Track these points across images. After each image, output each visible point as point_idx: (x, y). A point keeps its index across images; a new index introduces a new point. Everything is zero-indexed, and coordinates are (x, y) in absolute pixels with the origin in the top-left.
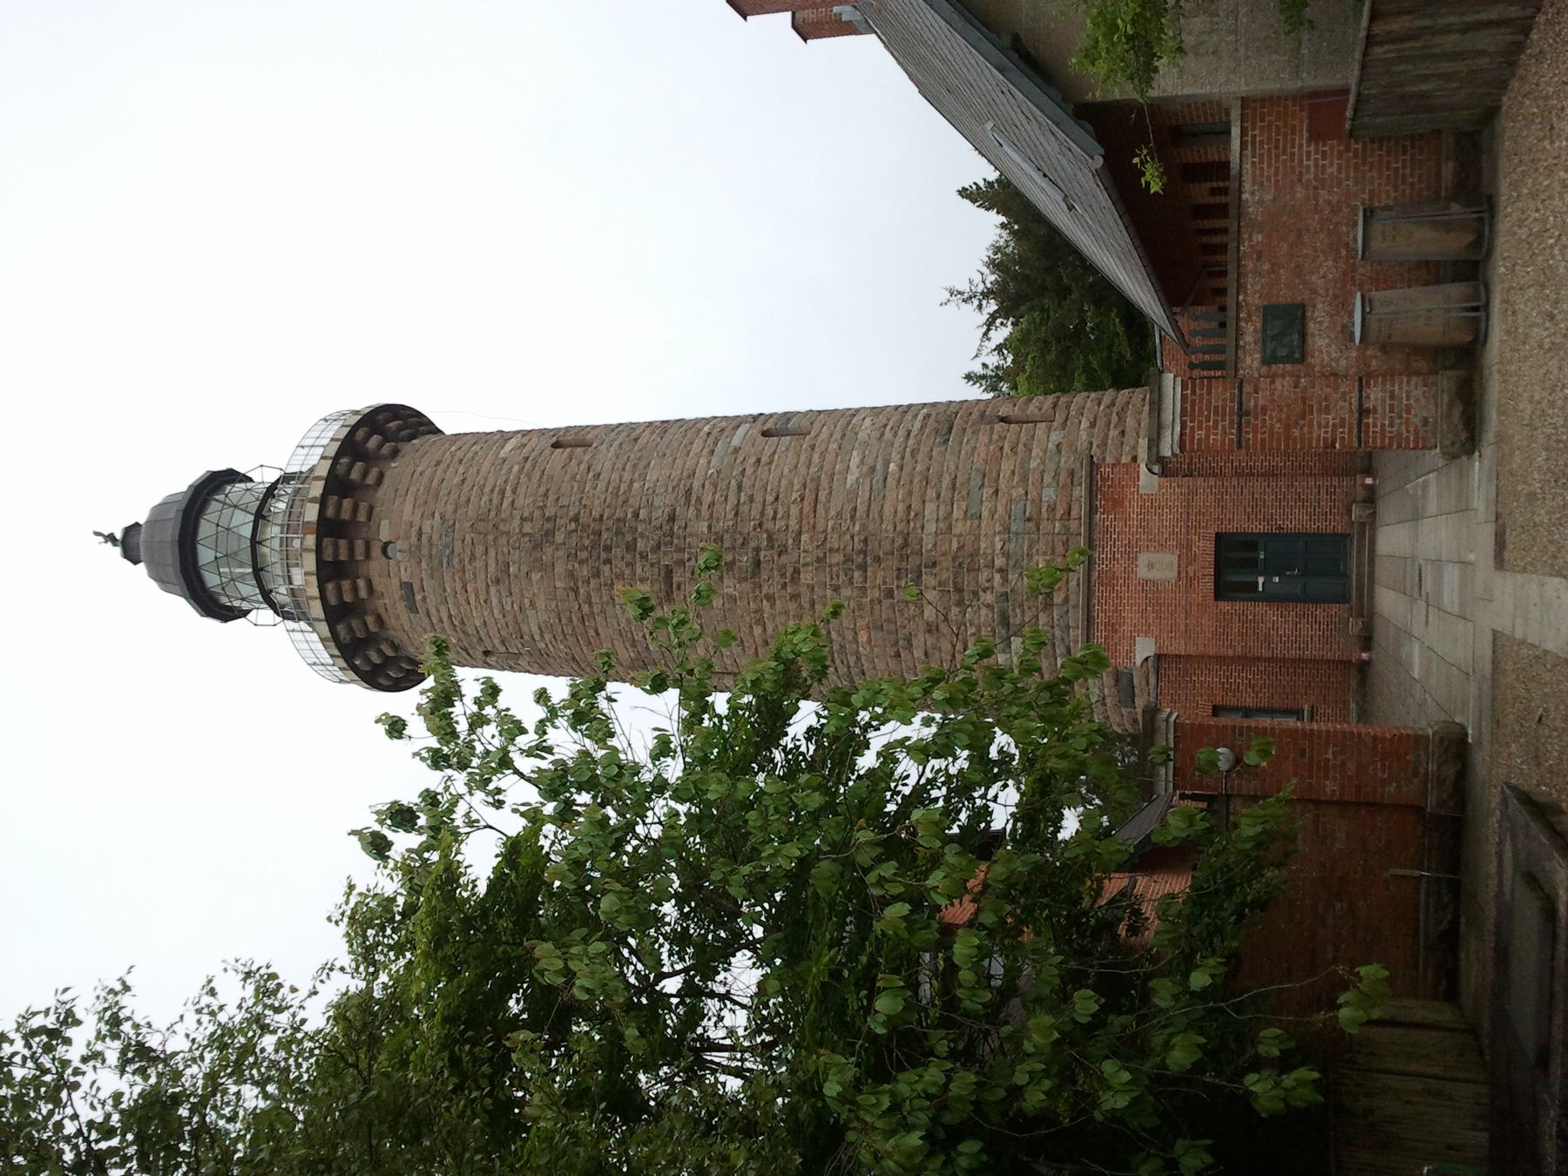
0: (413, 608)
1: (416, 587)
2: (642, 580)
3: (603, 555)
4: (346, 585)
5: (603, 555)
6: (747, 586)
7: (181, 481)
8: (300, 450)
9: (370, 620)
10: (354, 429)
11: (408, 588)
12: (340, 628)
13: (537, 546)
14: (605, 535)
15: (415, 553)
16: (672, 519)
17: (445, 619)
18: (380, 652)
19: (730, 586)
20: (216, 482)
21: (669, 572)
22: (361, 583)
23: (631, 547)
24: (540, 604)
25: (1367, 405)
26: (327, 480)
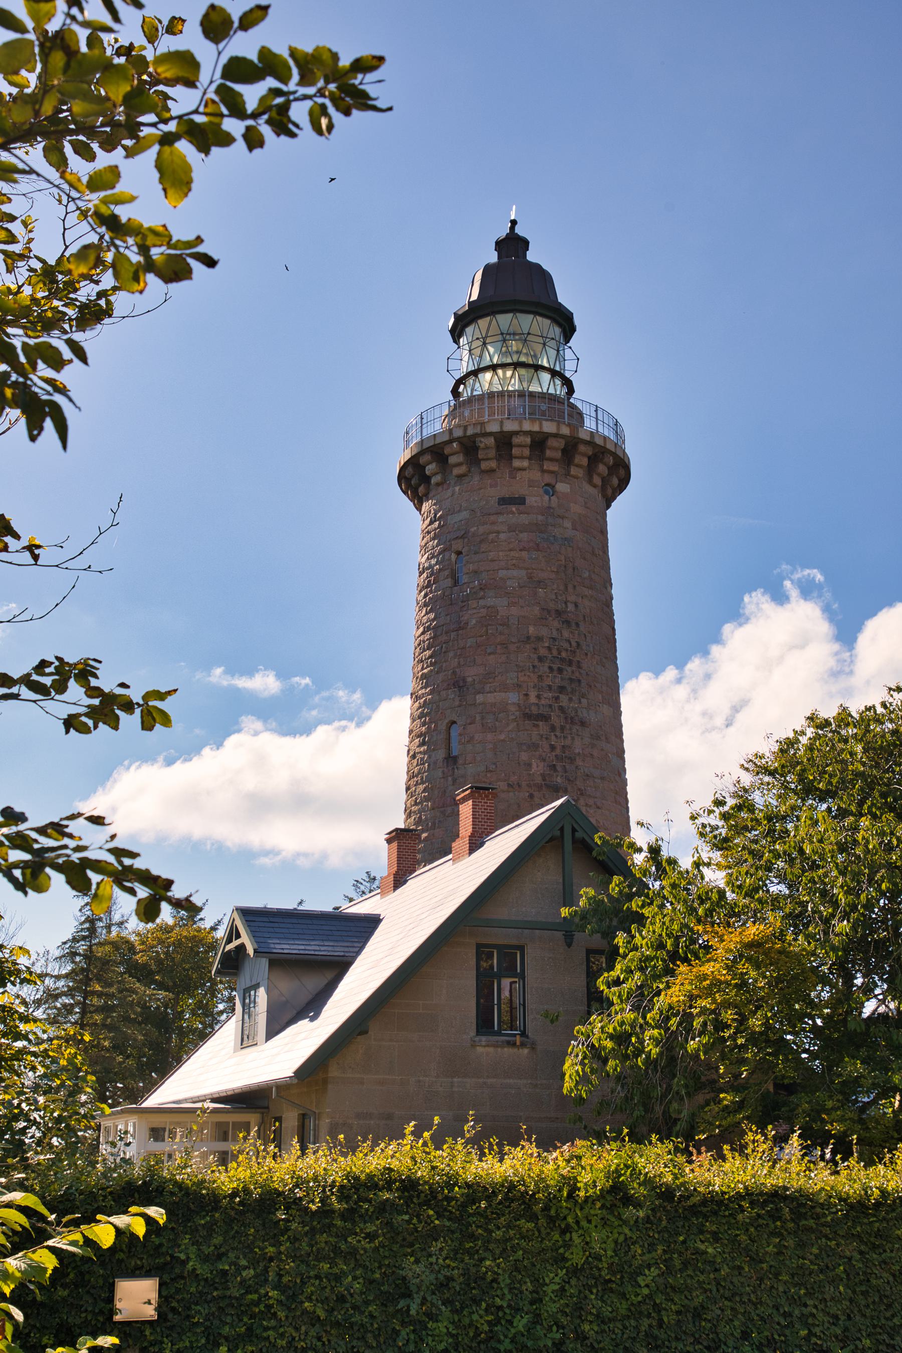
0: (503, 501)
1: (522, 507)
2: (538, 697)
3: (555, 667)
4: (527, 452)
5: (555, 667)
6: (539, 780)
7: (564, 297)
8: (593, 409)
9: (493, 464)
10: (614, 455)
11: (521, 501)
12: (491, 441)
13: (559, 613)
14: (569, 669)
15: (547, 511)
16: (583, 724)
17: (496, 528)
18: (459, 465)
19: (537, 768)
20: (566, 324)
21: (545, 718)
22: (525, 463)
23: (562, 689)
24: (514, 611)
25: (455, 753)
26: (604, 447)
